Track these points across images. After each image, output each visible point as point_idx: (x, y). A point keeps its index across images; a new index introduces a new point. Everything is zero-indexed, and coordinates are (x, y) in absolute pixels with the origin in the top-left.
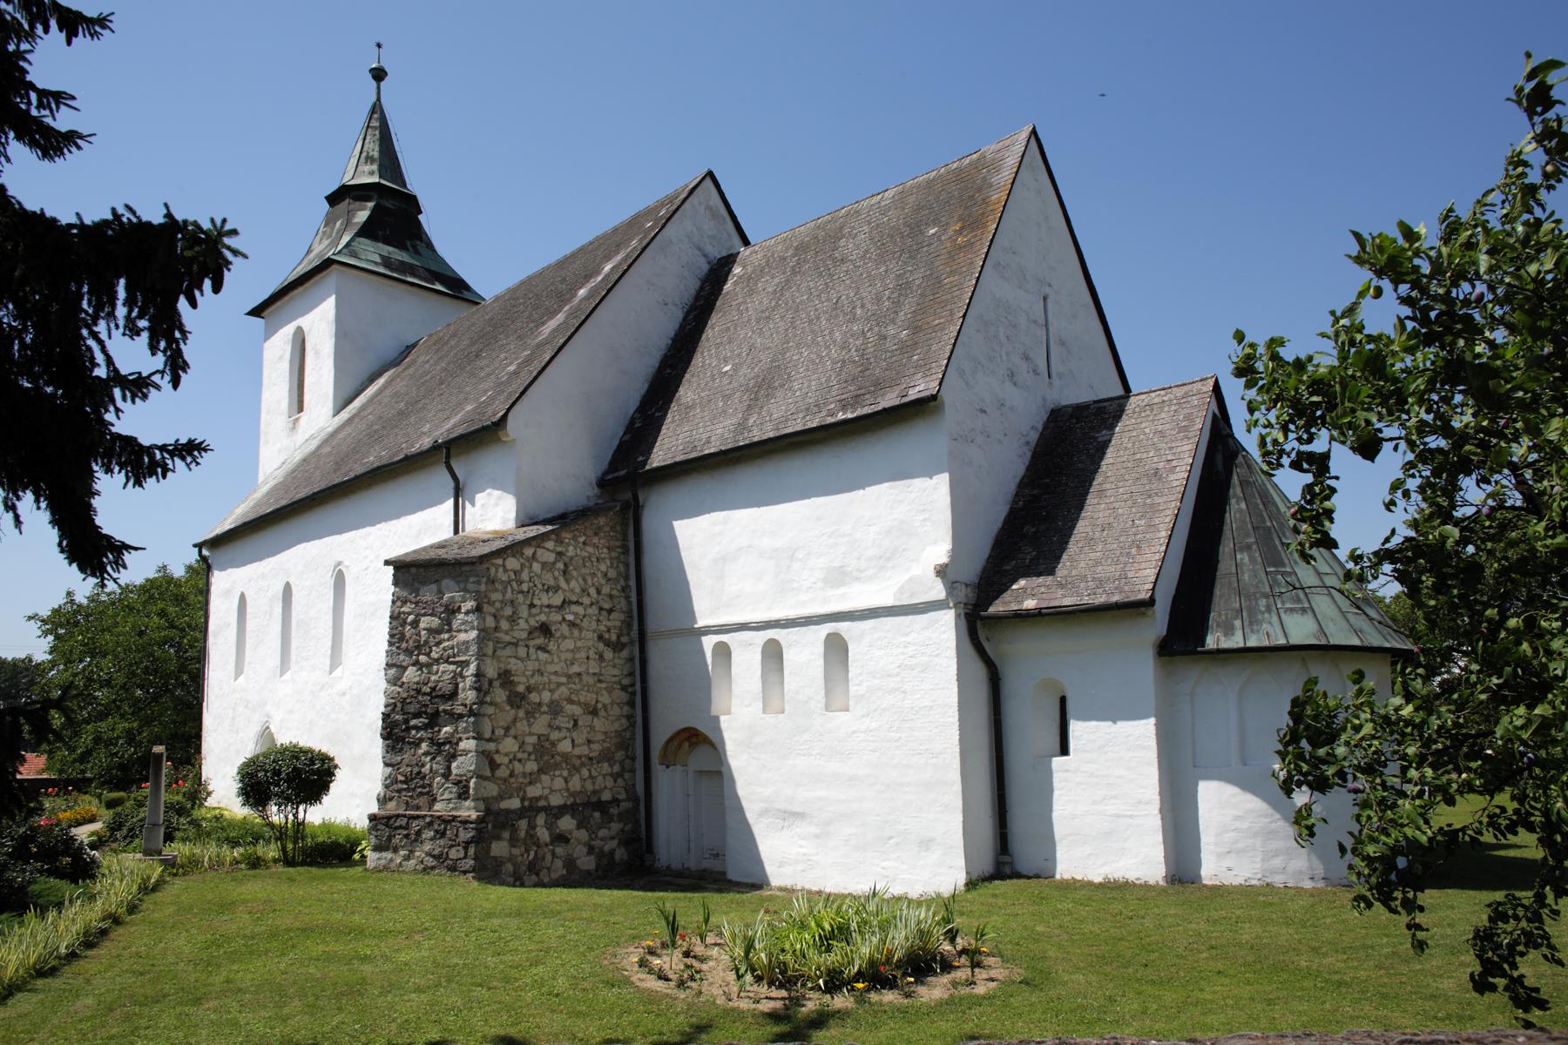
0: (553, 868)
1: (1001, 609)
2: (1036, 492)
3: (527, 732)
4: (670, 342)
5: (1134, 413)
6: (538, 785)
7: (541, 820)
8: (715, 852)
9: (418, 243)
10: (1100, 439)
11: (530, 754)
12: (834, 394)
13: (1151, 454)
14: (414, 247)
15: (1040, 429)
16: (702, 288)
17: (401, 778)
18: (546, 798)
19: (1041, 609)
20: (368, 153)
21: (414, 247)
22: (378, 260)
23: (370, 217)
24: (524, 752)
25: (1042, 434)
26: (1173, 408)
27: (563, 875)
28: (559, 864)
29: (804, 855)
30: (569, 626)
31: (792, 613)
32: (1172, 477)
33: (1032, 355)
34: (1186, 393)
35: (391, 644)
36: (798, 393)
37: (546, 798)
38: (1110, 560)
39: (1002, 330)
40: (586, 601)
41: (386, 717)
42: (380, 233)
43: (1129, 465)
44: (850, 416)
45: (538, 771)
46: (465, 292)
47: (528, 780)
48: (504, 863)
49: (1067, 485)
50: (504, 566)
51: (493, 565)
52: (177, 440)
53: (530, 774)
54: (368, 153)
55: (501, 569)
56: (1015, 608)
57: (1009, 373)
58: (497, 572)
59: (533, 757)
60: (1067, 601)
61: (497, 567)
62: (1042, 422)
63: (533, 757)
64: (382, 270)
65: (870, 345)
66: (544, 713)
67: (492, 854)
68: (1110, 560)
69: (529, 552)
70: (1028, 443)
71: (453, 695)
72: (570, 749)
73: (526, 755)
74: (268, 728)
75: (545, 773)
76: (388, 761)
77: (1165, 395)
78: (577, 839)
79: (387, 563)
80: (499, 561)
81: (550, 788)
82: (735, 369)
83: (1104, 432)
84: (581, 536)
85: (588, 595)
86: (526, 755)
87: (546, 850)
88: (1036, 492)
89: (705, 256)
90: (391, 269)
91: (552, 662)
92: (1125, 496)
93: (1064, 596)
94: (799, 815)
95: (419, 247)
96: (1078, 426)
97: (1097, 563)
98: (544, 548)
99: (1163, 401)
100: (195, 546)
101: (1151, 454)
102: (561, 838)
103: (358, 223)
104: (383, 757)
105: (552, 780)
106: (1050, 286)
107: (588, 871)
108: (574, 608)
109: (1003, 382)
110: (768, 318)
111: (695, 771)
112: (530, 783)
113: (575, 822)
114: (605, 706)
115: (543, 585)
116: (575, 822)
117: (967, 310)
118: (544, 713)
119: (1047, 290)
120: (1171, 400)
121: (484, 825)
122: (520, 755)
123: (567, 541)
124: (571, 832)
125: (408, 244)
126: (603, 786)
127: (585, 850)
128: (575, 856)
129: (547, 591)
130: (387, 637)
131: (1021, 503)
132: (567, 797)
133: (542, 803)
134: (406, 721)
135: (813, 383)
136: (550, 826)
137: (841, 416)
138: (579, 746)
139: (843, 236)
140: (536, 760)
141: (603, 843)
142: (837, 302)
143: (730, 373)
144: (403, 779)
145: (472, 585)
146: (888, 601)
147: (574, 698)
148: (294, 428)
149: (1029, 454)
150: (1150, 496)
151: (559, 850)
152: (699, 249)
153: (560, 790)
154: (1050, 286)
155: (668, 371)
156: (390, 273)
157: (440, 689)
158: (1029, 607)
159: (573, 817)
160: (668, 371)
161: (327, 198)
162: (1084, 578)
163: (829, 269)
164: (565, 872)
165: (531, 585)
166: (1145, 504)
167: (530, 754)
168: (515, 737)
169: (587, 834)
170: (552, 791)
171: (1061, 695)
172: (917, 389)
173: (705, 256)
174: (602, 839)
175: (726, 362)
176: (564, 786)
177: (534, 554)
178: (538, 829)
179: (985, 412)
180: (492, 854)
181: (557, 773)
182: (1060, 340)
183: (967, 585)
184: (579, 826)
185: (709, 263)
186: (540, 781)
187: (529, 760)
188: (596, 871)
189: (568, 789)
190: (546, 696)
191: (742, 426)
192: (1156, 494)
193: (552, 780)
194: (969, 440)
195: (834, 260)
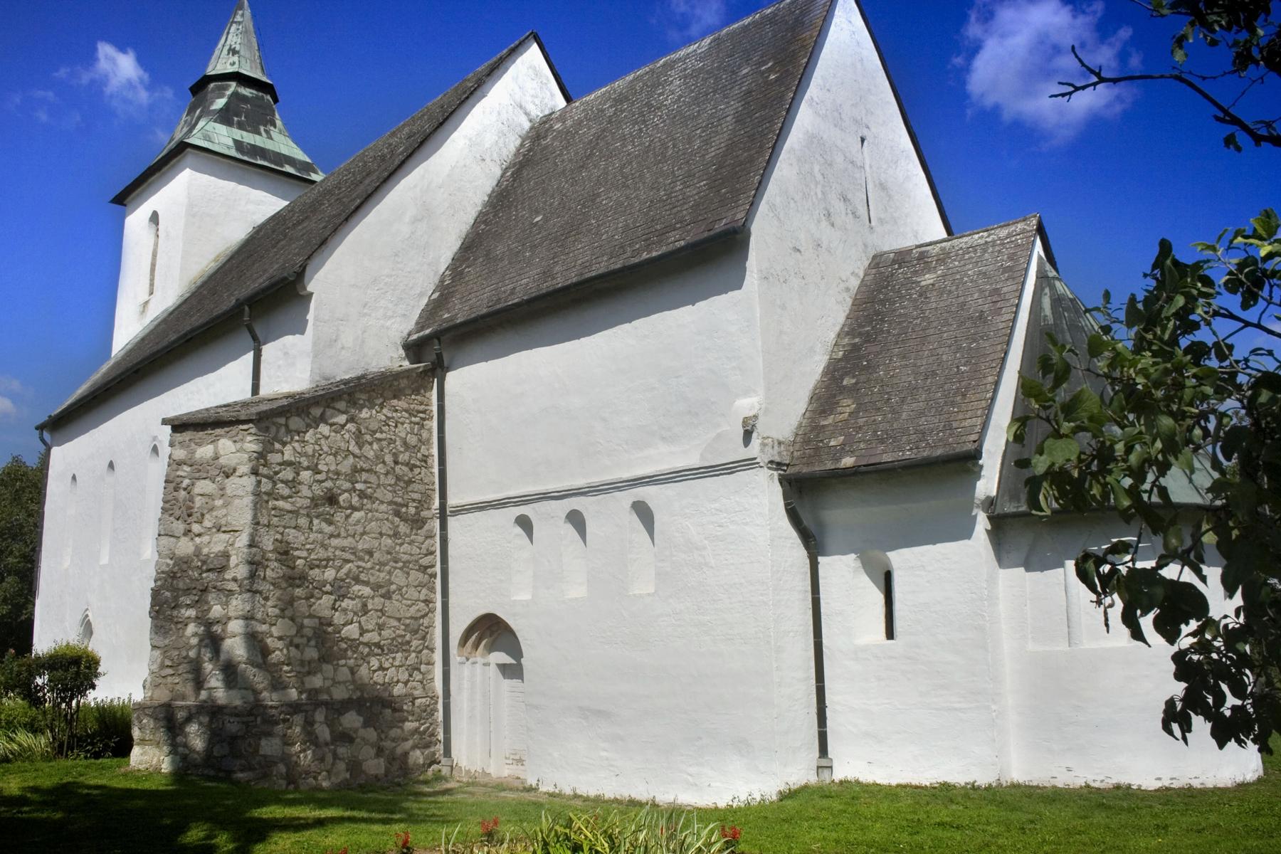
0: (335, 770)
1: (817, 469)
2: (857, 340)
3: (307, 614)
4: (486, 199)
5: (957, 255)
6: (319, 676)
7: (320, 716)
8: (517, 757)
9: (272, 128)
10: (923, 283)
11: (309, 640)
12: (640, 235)
13: (976, 296)
14: (267, 132)
15: (861, 274)
16: (522, 145)
17: (168, 663)
18: (328, 691)
19: (860, 466)
20: (231, 46)
21: (267, 132)
22: (231, 143)
23: (227, 104)
24: (302, 636)
25: (863, 280)
26: (997, 248)
27: (347, 780)
28: (341, 766)
29: (607, 759)
30: (359, 495)
31: (595, 480)
32: (999, 319)
33: (849, 196)
34: (1009, 233)
35: (164, 510)
36: (604, 237)
37: (328, 691)
38: (933, 410)
39: (817, 168)
40: (380, 468)
41: (156, 593)
42: (236, 119)
43: (953, 309)
44: (654, 254)
45: (319, 659)
46: (312, 174)
47: (306, 669)
48: (276, 763)
49: (888, 332)
50: (287, 426)
51: (274, 424)
52: (975, 782)
53: (309, 662)
54: (231, 46)
55: (283, 430)
56: (833, 467)
57: (825, 212)
58: (278, 432)
59: (313, 643)
60: (886, 458)
61: (278, 426)
62: (862, 268)
63: (313, 643)
64: (233, 153)
65: (678, 183)
66: (327, 593)
67: (261, 752)
68: (933, 410)
69: (316, 412)
70: (848, 289)
71: (223, 569)
72: (356, 636)
73: (304, 640)
74: (87, 616)
75: (327, 663)
76: (156, 644)
77: (988, 236)
78: (363, 739)
79: (165, 422)
80: (282, 420)
81: (333, 679)
82: (546, 220)
83: (927, 276)
84: (377, 398)
85: (384, 462)
86: (304, 640)
87: (326, 750)
88: (857, 340)
89: (527, 114)
90: (242, 152)
91: (338, 536)
92: (949, 342)
93: (884, 452)
94: (600, 713)
95: (272, 132)
96: (900, 271)
97: (921, 414)
98: (334, 408)
99: (986, 242)
100: (37, 428)
101: (976, 296)
102: (345, 737)
103: (215, 110)
104: (151, 639)
105: (335, 670)
106: (868, 127)
107: (376, 776)
108: (364, 476)
109: (819, 222)
110: (582, 167)
111: (498, 665)
112: (309, 673)
113: (361, 719)
114: (400, 588)
115: (331, 448)
116: (361, 719)
117: (776, 141)
118: (327, 593)
119: (865, 133)
120: (994, 241)
121: (252, 718)
122: (297, 640)
123: (361, 402)
124: (356, 731)
125: (262, 128)
126: (395, 679)
127: (373, 752)
128: (360, 758)
129: (335, 455)
130: (161, 504)
131: (841, 353)
132: (354, 691)
133: (325, 697)
134: (176, 598)
135: (620, 225)
136: (330, 723)
137: (645, 256)
138: (368, 631)
139: (660, 84)
140: (316, 647)
141: (394, 745)
142: (650, 145)
143: (540, 223)
144: (170, 664)
145: (249, 445)
146: (694, 461)
147: (363, 577)
148: (143, 311)
149: (849, 301)
150: (975, 341)
151: (342, 751)
152: (521, 107)
153: (344, 682)
154: (868, 127)
155: (483, 227)
156: (246, 158)
157: (212, 562)
158: (848, 465)
159: (359, 713)
160: (483, 227)
161: (191, 89)
162: (905, 431)
163: (644, 116)
164: (348, 776)
165: (317, 448)
166: (971, 349)
167: (309, 640)
168: (292, 619)
169: (375, 734)
170: (335, 683)
171: (886, 570)
172: (724, 221)
173: (527, 114)
174: (393, 740)
175: (537, 213)
176: (350, 677)
177: (323, 414)
178: (316, 726)
179: (799, 250)
180: (261, 752)
181: (342, 662)
182: (881, 184)
183: (780, 443)
184: (366, 724)
185: (531, 121)
186: (321, 671)
187: (307, 645)
188: (386, 776)
189: (354, 682)
190: (330, 574)
191: (547, 274)
192: (982, 338)
193: (335, 670)
194: (782, 280)
195: (649, 105)
